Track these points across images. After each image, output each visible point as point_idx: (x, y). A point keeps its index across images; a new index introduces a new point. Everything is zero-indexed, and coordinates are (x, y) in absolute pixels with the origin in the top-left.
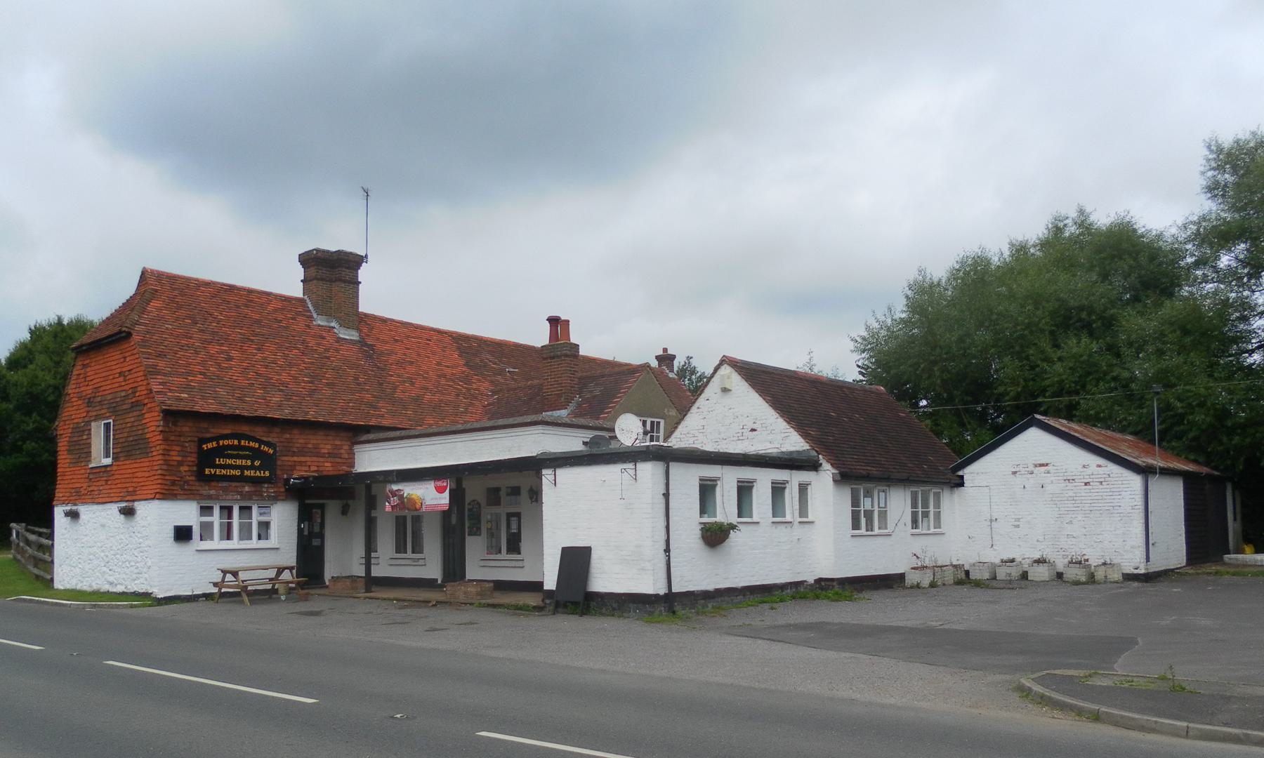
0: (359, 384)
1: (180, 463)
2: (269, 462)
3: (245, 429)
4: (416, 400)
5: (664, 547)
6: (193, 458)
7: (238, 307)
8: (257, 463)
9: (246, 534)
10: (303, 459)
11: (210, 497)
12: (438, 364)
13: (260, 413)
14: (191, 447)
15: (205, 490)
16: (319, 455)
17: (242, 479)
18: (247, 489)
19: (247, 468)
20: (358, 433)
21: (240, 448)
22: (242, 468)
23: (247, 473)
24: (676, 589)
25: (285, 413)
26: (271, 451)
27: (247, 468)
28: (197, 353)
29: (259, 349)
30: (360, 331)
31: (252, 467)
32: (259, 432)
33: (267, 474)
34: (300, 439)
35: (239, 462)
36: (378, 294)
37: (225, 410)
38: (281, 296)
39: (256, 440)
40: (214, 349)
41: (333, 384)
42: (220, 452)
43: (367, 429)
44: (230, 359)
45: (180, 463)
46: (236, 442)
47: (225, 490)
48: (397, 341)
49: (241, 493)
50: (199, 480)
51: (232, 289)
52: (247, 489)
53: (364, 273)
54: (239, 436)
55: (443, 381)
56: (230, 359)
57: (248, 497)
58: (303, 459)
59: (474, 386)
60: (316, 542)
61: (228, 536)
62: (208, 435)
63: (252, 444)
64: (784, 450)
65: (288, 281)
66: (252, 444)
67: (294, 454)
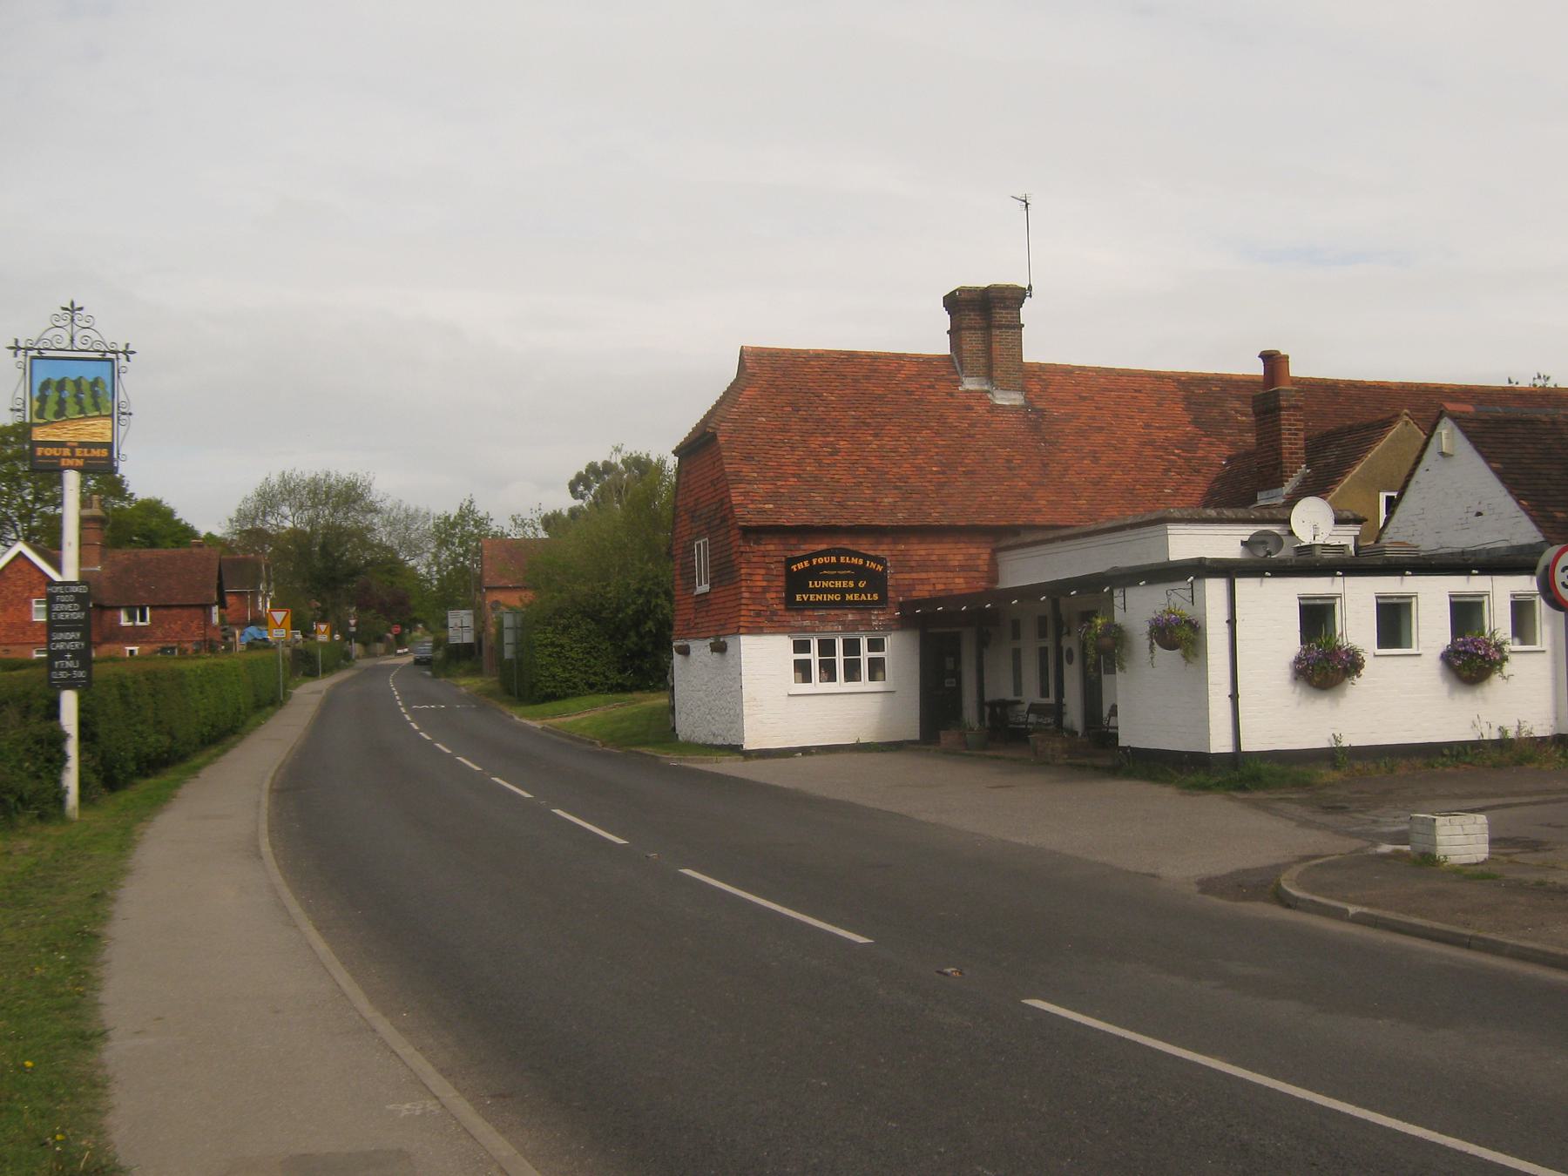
0: (1009, 469)
1: (765, 590)
2: (877, 582)
3: (845, 543)
4: (1097, 484)
5: (1229, 692)
6: (780, 583)
7: (856, 381)
8: (862, 584)
9: (852, 673)
10: (924, 575)
11: (804, 630)
12: (1147, 426)
13: (863, 521)
14: (778, 569)
15: (796, 620)
16: (946, 568)
17: (843, 605)
18: (850, 617)
19: (850, 590)
20: (1005, 536)
21: (838, 566)
22: (843, 591)
23: (849, 597)
24: (1252, 742)
25: (901, 517)
26: (880, 568)
27: (850, 590)
28: (793, 449)
29: (876, 435)
30: (1023, 389)
31: (856, 590)
32: (864, 546)
33: (876, 597)
34: (918, 550)
35: (838, 584)
36: (1045, 340)
37: (817, 521)
38: (918, 357)
39: (857, 554)
40: (815, 443)
41: (972, 472)
42: (814, 572)
43: (1014, 530)
44: (835, 452)
45: (765, 590)
46: (834, 559)
47: (822, 619)
48: (1083, 399)
49: (843, 623)
50: (787, 609)
51: (851, 357)
52: (850, 617)
53: (1027, 311)
54: (839, 552)
55: (1148, 451)
56: (835, 452)
57: (853, 627)
58: (924, 575)
59: (1200, 453)
60: (949, 683)
61: (832, 677)
62: (798, 554)
63: (855, 561)
64: (1514, 543)
65: (931, 335)
66: (855, 561)
67: (912, 569)
